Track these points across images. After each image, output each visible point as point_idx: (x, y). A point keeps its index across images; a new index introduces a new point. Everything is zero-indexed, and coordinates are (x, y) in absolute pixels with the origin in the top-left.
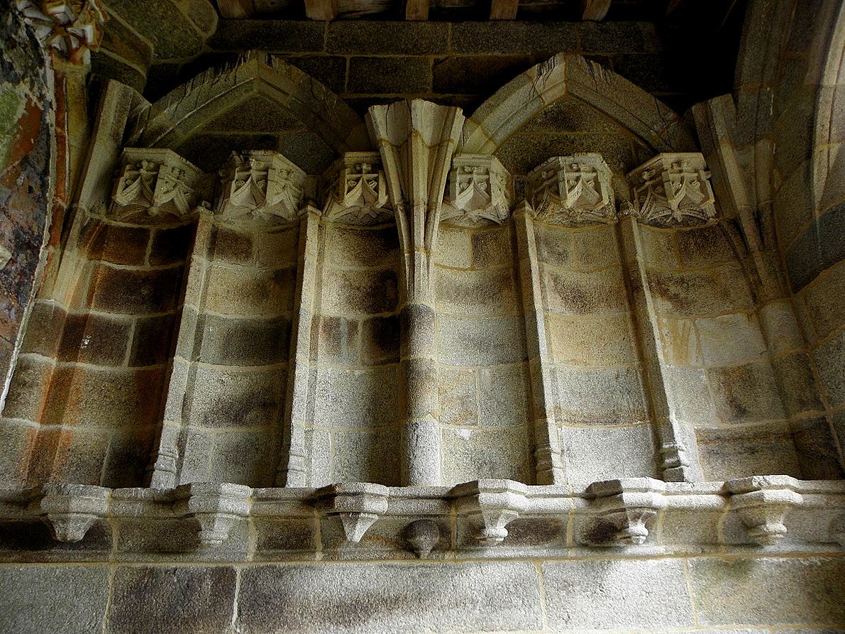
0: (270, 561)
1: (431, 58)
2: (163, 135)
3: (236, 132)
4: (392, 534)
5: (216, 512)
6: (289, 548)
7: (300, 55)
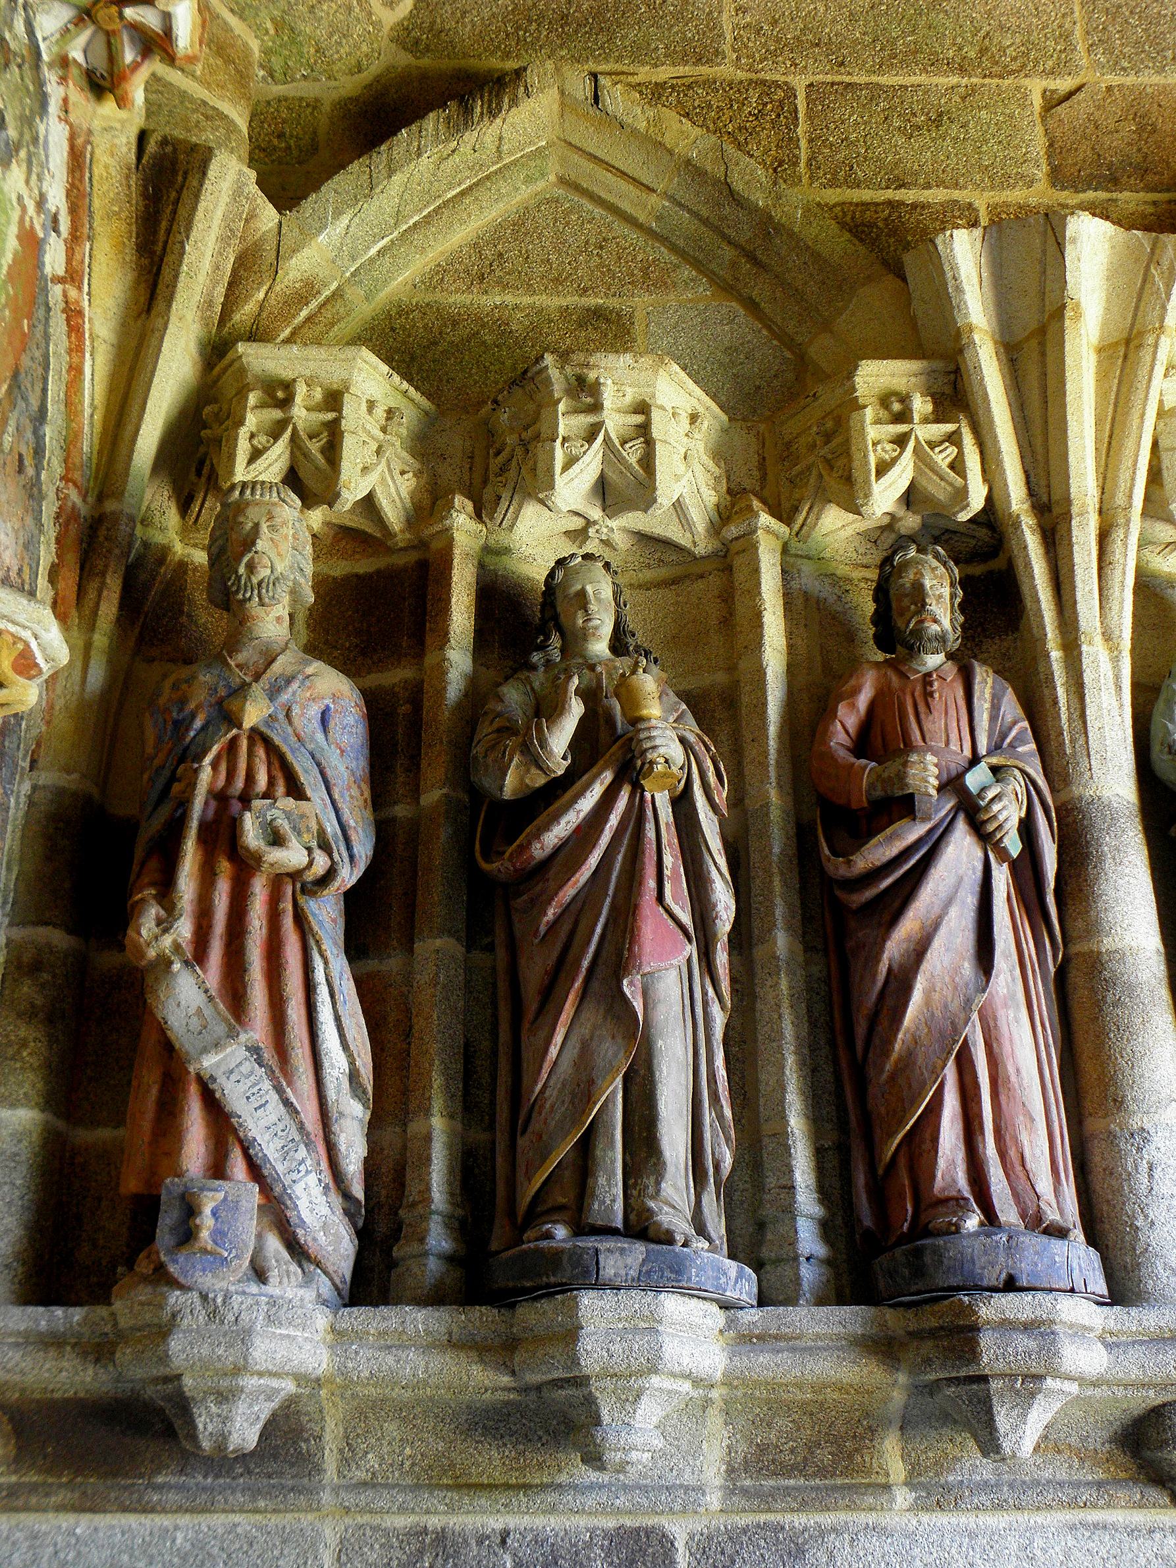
0: (769, 1510)
1: (1036, 87)
2: (314, 305)
3: (510, 299)
4: (1098, 1439)
5: (654, 1370)
6: (814, 1475)
7: (664, 73)
